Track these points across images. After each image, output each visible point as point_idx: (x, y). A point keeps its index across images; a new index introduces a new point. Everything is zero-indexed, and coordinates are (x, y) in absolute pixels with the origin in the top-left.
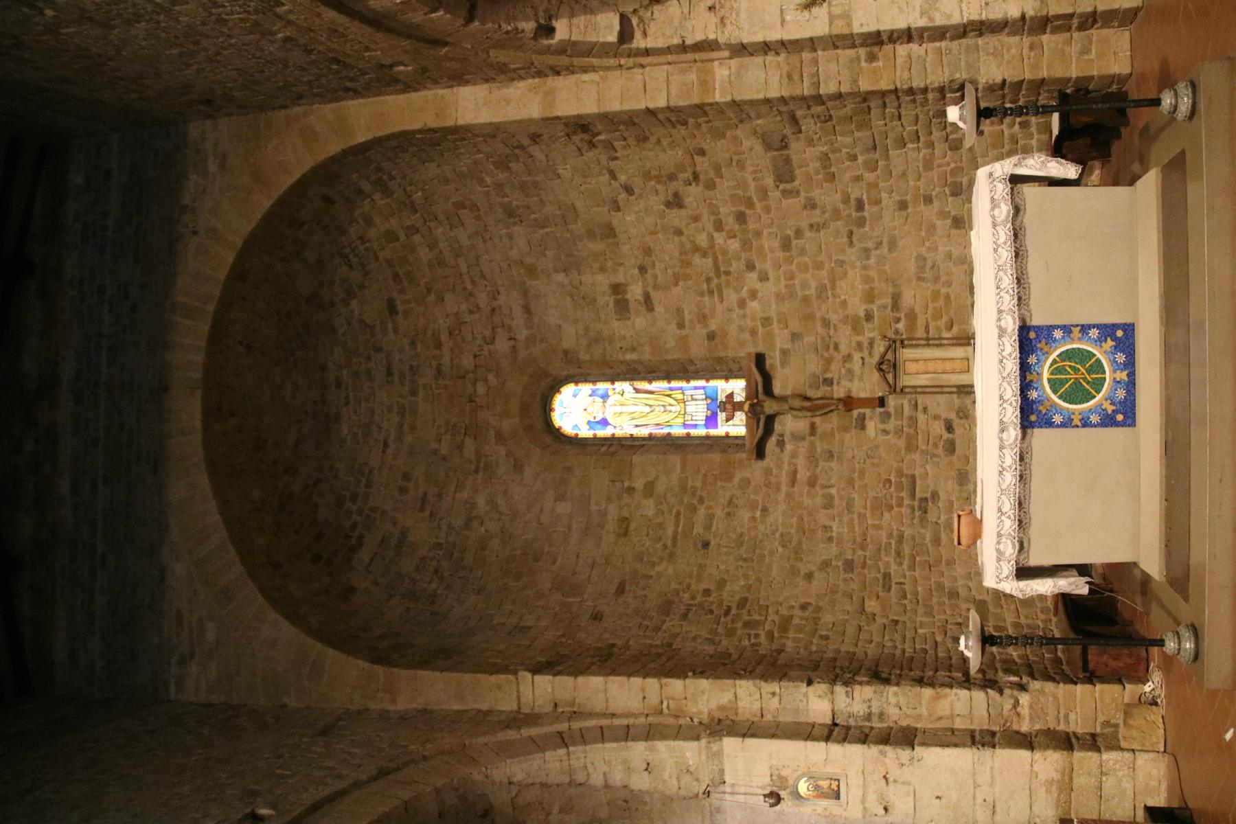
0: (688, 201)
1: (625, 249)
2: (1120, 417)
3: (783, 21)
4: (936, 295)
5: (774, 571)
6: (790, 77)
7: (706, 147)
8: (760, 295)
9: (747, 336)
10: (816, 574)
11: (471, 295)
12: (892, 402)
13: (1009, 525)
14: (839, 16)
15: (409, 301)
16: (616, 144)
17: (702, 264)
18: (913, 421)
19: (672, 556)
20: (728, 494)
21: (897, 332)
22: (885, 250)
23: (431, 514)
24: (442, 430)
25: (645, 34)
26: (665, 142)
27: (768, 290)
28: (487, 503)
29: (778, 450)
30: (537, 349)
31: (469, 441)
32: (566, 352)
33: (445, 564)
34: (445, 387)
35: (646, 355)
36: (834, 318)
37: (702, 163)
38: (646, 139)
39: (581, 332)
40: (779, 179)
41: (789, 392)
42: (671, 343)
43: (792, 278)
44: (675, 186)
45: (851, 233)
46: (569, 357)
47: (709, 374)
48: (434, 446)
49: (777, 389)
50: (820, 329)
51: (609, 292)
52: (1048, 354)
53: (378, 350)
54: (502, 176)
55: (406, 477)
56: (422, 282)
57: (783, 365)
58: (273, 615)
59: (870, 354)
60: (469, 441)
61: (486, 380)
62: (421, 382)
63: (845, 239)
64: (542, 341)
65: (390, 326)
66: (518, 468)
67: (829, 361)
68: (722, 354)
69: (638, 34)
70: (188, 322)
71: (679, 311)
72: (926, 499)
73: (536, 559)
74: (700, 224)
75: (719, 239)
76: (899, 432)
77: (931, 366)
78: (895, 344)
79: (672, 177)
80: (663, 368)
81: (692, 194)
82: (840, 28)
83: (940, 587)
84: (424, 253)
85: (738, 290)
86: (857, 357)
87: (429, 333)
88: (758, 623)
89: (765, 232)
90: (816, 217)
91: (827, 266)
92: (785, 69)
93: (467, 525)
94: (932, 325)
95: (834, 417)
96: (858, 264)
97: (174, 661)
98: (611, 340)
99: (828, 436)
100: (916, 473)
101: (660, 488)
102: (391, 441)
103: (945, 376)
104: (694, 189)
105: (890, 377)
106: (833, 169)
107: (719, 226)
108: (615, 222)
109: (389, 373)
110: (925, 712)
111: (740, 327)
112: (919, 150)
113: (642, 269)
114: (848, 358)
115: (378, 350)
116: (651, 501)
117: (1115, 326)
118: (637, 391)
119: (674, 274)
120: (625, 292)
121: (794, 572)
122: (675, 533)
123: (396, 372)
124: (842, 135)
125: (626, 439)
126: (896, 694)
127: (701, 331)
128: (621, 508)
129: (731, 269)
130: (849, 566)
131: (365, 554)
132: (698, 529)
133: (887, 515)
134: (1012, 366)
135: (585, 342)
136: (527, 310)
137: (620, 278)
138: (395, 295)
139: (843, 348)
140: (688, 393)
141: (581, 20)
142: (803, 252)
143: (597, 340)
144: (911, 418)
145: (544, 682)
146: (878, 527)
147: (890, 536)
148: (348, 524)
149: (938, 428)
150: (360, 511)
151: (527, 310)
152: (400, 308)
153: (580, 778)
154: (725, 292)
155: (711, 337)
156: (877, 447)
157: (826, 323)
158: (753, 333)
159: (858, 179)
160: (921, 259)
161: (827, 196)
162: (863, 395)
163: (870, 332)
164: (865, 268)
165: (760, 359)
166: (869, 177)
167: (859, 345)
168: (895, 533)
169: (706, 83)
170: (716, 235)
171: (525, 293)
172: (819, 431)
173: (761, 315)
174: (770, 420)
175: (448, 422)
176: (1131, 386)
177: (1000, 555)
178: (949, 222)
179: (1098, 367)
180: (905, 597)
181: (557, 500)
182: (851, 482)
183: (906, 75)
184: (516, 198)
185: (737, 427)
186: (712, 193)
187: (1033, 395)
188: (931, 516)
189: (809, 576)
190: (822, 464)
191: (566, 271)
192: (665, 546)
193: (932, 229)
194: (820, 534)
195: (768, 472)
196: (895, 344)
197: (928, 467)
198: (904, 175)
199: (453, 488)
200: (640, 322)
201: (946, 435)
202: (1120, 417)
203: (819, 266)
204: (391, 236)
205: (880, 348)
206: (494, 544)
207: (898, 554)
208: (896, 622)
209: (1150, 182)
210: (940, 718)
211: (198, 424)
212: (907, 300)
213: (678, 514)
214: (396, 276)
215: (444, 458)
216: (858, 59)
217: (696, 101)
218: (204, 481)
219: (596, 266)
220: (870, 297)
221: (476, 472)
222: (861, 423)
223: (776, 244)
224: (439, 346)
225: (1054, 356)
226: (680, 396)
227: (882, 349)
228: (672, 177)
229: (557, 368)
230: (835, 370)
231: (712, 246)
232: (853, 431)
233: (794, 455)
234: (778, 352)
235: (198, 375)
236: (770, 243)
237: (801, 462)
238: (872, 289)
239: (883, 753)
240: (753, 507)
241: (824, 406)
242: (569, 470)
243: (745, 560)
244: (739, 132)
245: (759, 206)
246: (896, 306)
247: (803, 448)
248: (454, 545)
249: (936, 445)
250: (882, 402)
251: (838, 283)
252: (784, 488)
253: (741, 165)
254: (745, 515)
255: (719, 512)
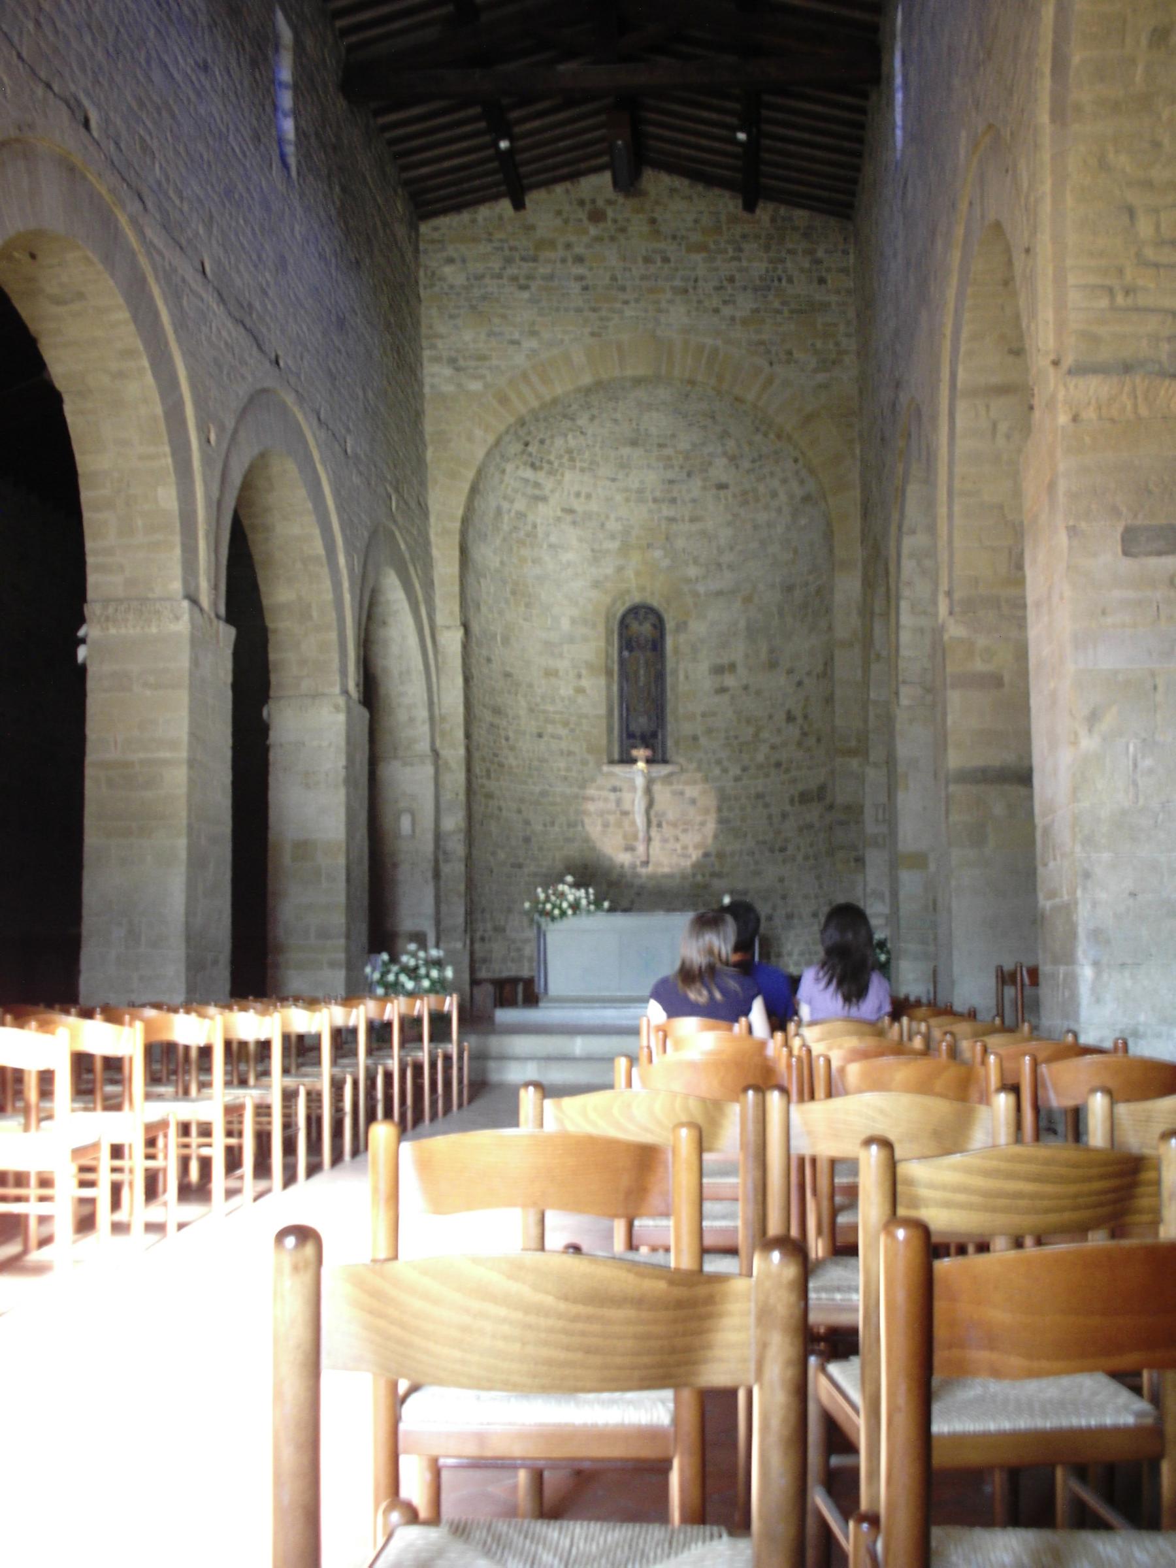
15: (726, 499)
32: (685, 623)
53: (689, 475)
67: (674, 825)
93: (550, 546)
104: (797, 732)
107: (773, 747)
114: (677, 839)
115: (689, 475)
116: (571, 692)
130: (527, 840)
132: (550, 729)
206: (537, 571)
215: (603, 525)
223: (760, 789)
230: (667, 831)
233: (606, 800)
240: (568, 769)
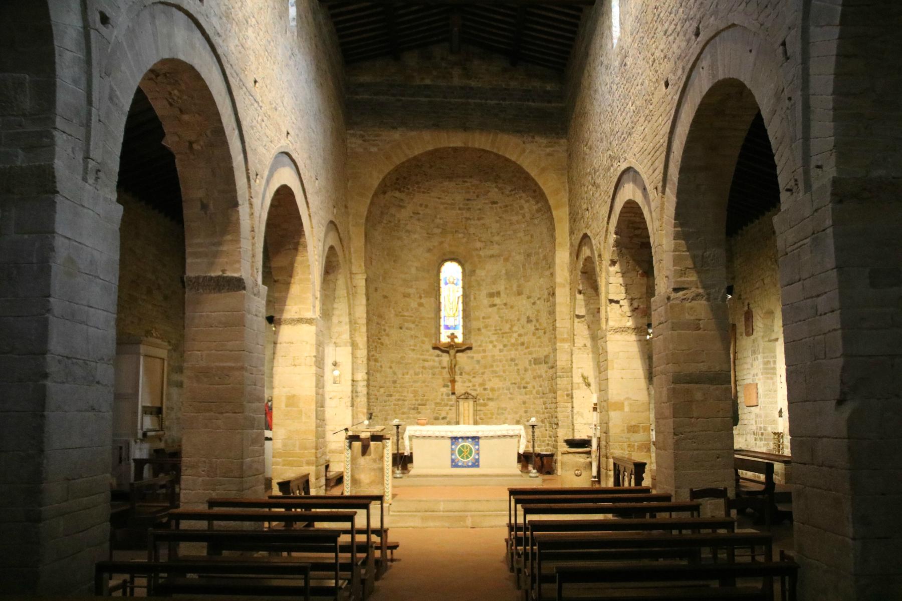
0: (529, 325)
1: (513, 298)
2: (454, 464)
3: (579, 368)
4: (492, 414)
5: (393, 355)
6: (563, 368)
7: (546, 335)
8: (494, 349)
9: (479, 343)
10: (391, 370)
11: (498, 234)
12: (454, 397)
13: (424, 434)
14: (579, 386)
16: (549, 303)
17: (507, 327)
18: (446, 405)
19: (396, 315)
20: (419, 336)
21: (479, 400)
22: (509, 396)
23: (411, 217)
24: (445, 220)
25: (579, 322)
26: (548, 320)
27: (496, 352)
28: (415, 239)
29: (436, 354)
30: (476, 259)
31: (440, 230)
32: (474, 271)
33: (392, 224)
34: (462, 222)
35: (473, 304)
36: (485, 376)
37: (541, 332)
38: (550, 314)
39: (482, 278)
40: (535, 359)
41: (457, 359)
42: (477, 314)
43: (500, 362)
44: (534, 322)
45: (515, 384)
46: (473, 272)
47: (465, 327)
48: (438, 216)
49: (459, 354)
50: (481, 371)
51: (497, 290)
52: (471, 444)
53: (478, 196)
54: (541, 256)
55: (426, 206)
56: (504, 216)
57: (468, 357)
58: (381, 177)
59: (471, 390)
60: (440, 230)
61: (464, 237)
62: (464, 212)
63: (513, 382)
64: (480, 261)
65: (487, 201)
66: (429, 250)
67: (469, 374)
68: (473, 333)
69: (579, 320)
70: (490, 141)
71: (489, 318)
72: (418, 409)
73: (394, 261)
74: (521, 328)
75: (515, 335)
76: (442, 400)
77: (466, 412)
78: (475, 399)
79: (537, 320)
80: (467, 309)
81: (531, 327)
82: (575, 386)
83: (388, 414)
84: (514, 218)
85: (497, 341)
86: (470, 384)
87: (483, 216)
88: (376, 350)
89: (517, 352)
90: (522, 372)
91: (504, 374)
92: (566, 367)
93: (407, 231)
94: (482, 412)
95: (448, 376)
96: (504, 386)
97: (362, 132)
98: (479, 290)
99: (441, 373)
100: (427, 406)
101: (421, 309)
102: (441, 200)
103: (463, 417)
105: (463, 397)
106: (537, 379)
108: (523, 296)
109: (468, 200)
110: (359, 409)
111: (482, 341)
112: (542, 409)
113: (505, 304)
114: (470, 381)
115: (478, 196)
117: (478, 462)
118: (459, 298)
119: (503, 317)
120: (497, 297)
121: (392, 362)
122: (405, 316)
123: (468, 202)
124: (548, 383)
125: (439, 293)
126: (364, 401)
127: (481, 325)
128: (414, 294)
129: (504, 339)
130: (395, 382)
131: (397, 194)
133: (412, 395)
134: (468, 435)
135: (478, 279)
136: (492, 256)
137: (502, 295)
138: (499, 205)
139: (474, 380)
140: (457, 318)
141: (583, 303)
142: (510, 366)
143: (479, 284)
144: (447, 404)
145: (363, 283)
146: (408, 392)
147: (405, 396)
148: (409, 187)
149: (443, 414)
150: (414, 190)
151: (492, 256)
152: (494, 206)
153: (336, 300)
154: (496, 336)
155: (479, 330)
156: (437, 392)
157: (483, 373)
158: (480, 346)
159: (534, 387)
160: (505, 409)
161: (529, 376)
162: (456, 387)
163: (480, 390)
164: (503, 388)
165: (470, 348)
166: (534, 391)
167: (474, 386)
168: (405, 398)
169: (563, 340)
170: (517, 334)
171: (499, 256)
172: (443, 370)
173: (487, 349)
174: (448, 352)
175: (447, 222)
176: (462, 467)
177: (416, 431)
178: (518, 419)
179: (467, 457)
180: (385, 402)
181: (417, 268)
182: (424, 382)
183: (561, 406)
184: (533, 259)
185: (444, 339)
186: (532, 334)
187: (460, 440)
188: (412, 411)
189: (391, 367)
190: (431, 371)
191: (507, 274)
192: (400, 312)
193: (516, 413)
194: (406, 371)
195: (427, 351)
196: (475, 399)
197: (429, 410)
198: (535, 404)
199: (421, 225)
200: (486, 301)
201: (441, 417)
202: (454, 464)
203: (504, 372)
204: (522, 208)
205: (474, 393)
207: (399, 400)
208: (377, 399)
209: (520, 473)
210: (357, 415)
211: (451, 145)
212: (491, 404)
213: (412, 317)
214: (506, 206)
215: (433, 221)
216: (568, 391)
217: (558, 337)
218: (430, 148)
219: (508, 286)
220: (493, 390)
221: (427, 234)
222: (445, 386)
223: (513, 356)
224: (479, 219)
225: (471, 446)
226: (456, 315)
227: (473, 394)
228: (537, 320)
229: (468, 266)
231: (513, 332)
232: (443, 383)
233: (434, 361)
234: (472, 355)
235: (470, 145)
236: (513, 354)
237: (430, 364)
238: (495, 391)
239: (349, 397)
240: (415, 346)
241: (452, 372)
242: (428, 271)
243: (396, 343)
244: (550, 347)
245: (526, 351)
246: (489, 399)
247: (437, 364)
248: (399, 227)
249: (437, 413)
250: (453, 393)
251: (498, 378)
252: (422, 357)
253: (540, 346)
254: (412, 342)
255: (413, 332)
